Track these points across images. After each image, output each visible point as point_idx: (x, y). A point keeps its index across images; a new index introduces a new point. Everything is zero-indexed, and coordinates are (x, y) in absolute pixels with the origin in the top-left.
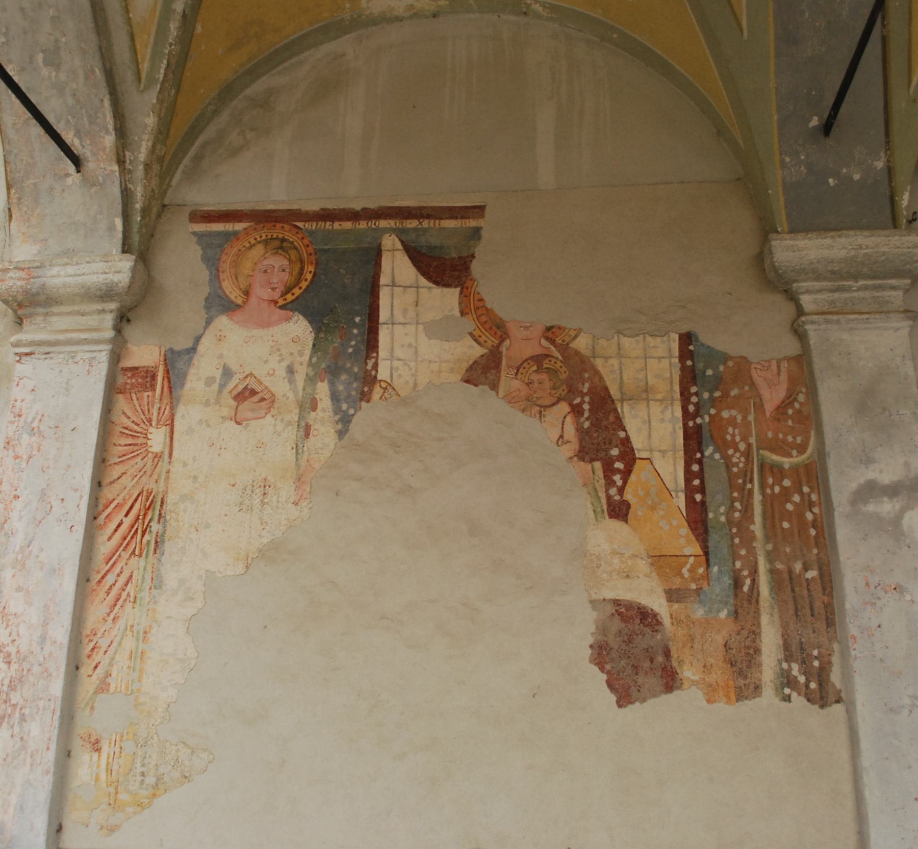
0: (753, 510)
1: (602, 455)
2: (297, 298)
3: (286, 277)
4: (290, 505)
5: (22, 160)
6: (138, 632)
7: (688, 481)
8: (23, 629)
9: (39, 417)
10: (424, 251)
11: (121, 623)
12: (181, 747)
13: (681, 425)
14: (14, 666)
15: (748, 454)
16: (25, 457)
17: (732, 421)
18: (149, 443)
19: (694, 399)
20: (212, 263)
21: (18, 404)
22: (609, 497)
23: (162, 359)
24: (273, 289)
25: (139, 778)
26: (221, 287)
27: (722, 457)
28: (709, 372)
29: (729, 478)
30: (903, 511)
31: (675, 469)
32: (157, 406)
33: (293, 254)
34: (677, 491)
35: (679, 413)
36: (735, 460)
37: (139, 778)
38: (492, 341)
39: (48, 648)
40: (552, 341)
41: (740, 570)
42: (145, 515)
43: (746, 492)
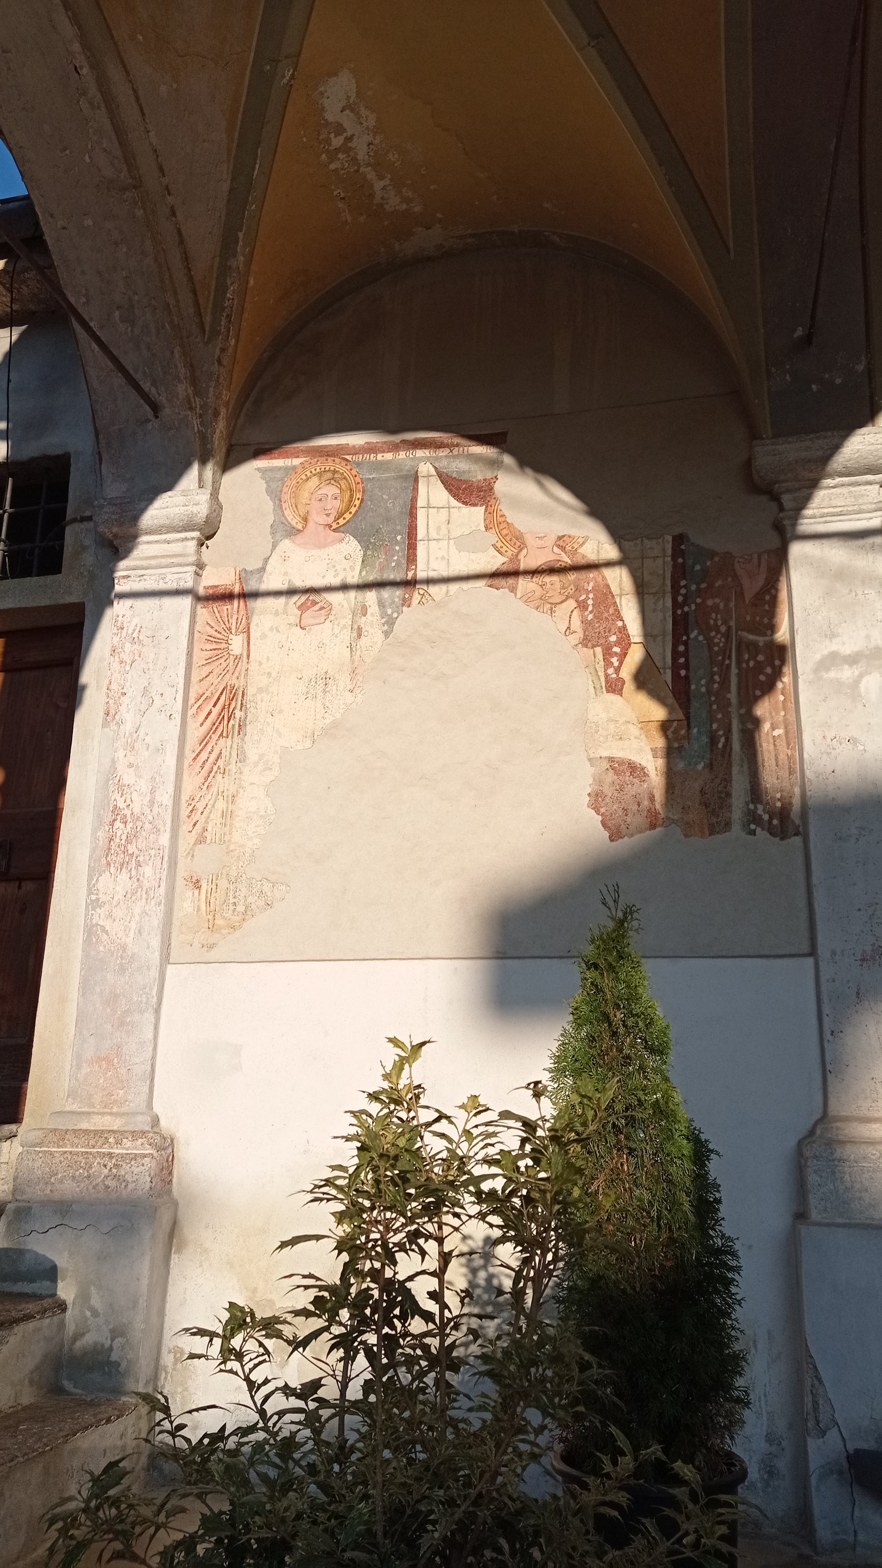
0: (730, 682)
1: (602, 641)
2: (348, 521)
3: (337, 504)
4: (347, 692)
5: (107, 408)
6: (228, 796)
7: (674, 659)
8: (135, 796)
9: (138, 629)
10: (454, 475)
11: (214, 790)
12: (264, 882)
13: (670, 613)
14: (129, 826)
15: (727, 636)
16: (128, 662)
17: (715, 609)
18: (230, 647)
19: (683, 591)
20: (276, 496)
21: (120, 619)
22: (607, 676)
23: (237, 578)
24: (328, 515)
25: (232, 908)
26: (283, 515)
27: (705, 639)
28: (698, 567)
29: (710, 656)
30: (861, 676)
31: (664, 651)
32: (235, 617)
33: (343, 483)
34: (664, 669)
35: (669, 603)
36: (716, 641)
37: (232, 908)
38: (511, 551)
39: (156, 810)
40: (563, 548)
41: (716, 731)
42: (229, 705)
43: (724, 667)
